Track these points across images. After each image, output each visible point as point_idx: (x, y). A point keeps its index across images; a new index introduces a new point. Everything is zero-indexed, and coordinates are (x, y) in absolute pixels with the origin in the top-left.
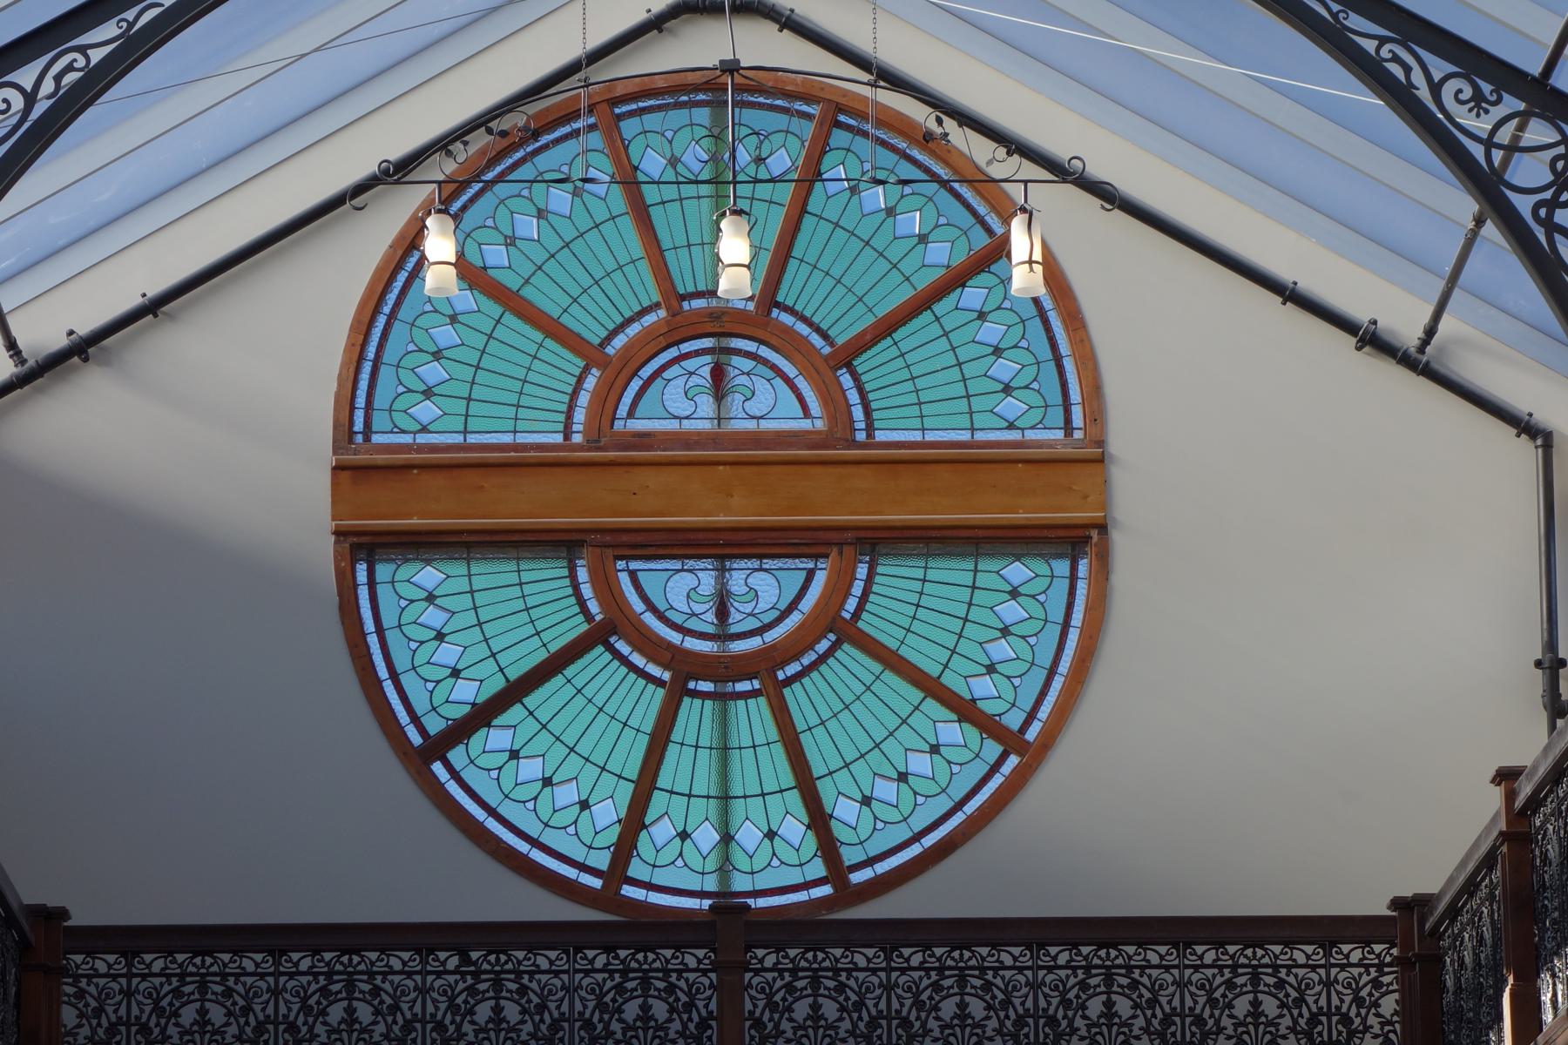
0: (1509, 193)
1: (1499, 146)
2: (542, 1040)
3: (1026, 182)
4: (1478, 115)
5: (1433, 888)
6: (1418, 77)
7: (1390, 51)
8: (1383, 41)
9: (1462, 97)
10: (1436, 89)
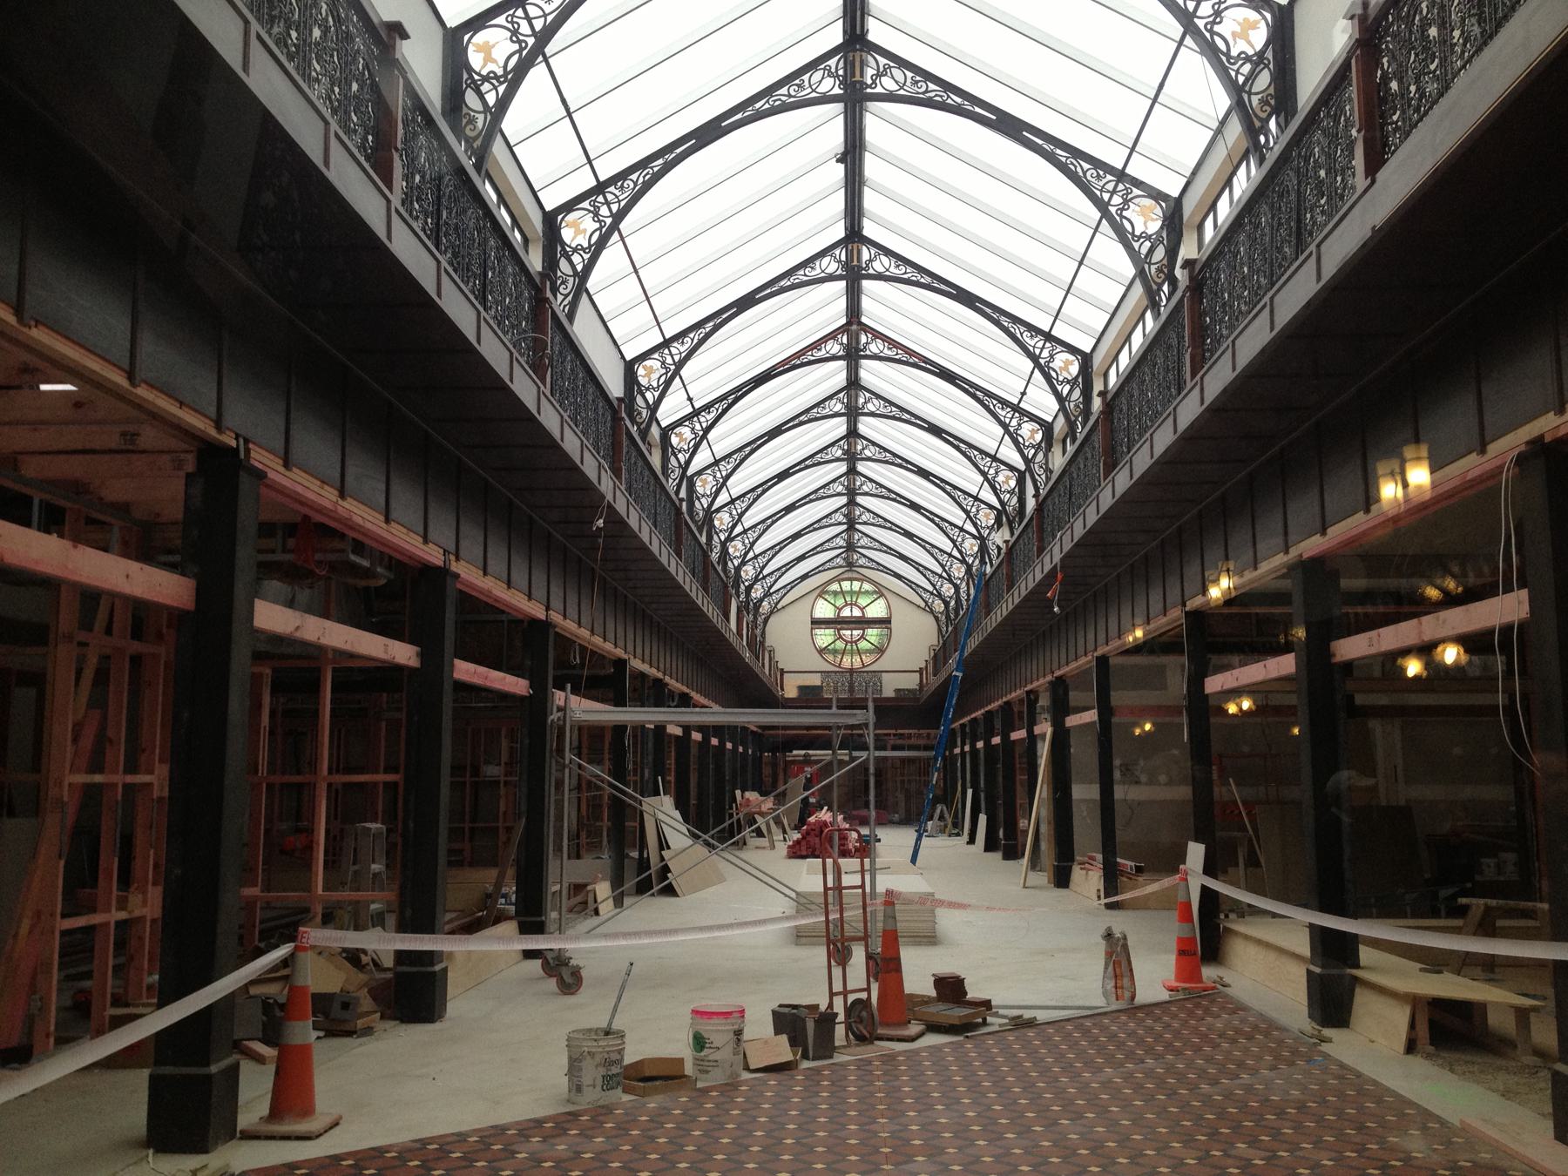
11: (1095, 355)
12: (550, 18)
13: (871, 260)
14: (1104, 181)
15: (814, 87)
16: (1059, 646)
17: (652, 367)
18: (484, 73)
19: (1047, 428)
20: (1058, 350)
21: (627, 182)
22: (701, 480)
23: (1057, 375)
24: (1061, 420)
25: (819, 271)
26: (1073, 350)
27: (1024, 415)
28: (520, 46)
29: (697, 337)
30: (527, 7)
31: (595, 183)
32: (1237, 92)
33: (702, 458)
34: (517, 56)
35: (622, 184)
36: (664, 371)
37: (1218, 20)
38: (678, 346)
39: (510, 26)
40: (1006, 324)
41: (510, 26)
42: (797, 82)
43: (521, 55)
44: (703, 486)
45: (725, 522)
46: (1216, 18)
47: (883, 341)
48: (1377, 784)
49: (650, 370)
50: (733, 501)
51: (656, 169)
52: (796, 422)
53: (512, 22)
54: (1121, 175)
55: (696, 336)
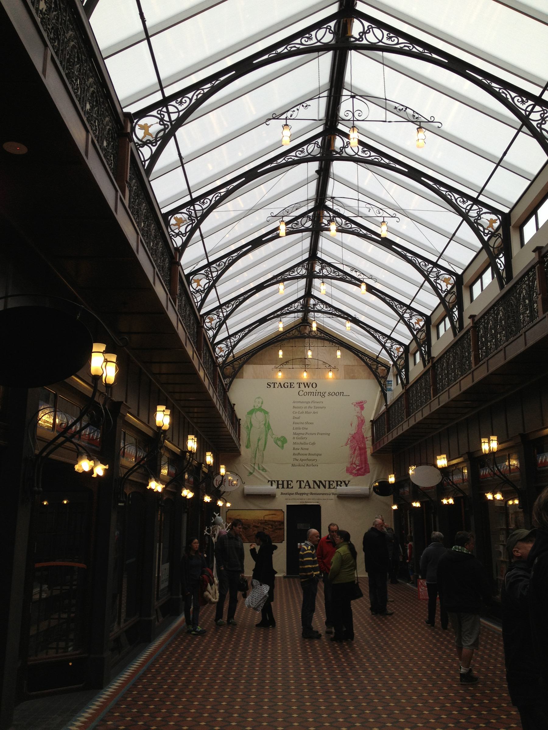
0: (430, 278)
1: (467, 210)
2: (313, 268)
3: (384, 217)
4: (523, 105)
5: (477, 314)
6: (453, 198)
7: (502, 91)
8: (447, 192)
9: (519, 101)
10: (456, 200)
11: (410, 346)
12: (181, 113)
13: (364, 33)
15: (296, 307)
18: (197, 289)
19: (407, 348)
20: (394, 344)
21: (230, 305)
22: (209, 318)
23: (394, 354)
24: (414, 344)
25: (314, 40)
26: (401, 344)
27: (379, 364)
29: (241, 335)
30: (169, 107)
31: (162, 98)
32: (443, 300)
33: (211, 304)
34: (219, 323)
35: (182, 99)
36: (219, 320)
37: (544, 122)
38: (233, 339)
39: (159, 116)
40: (372, 332)
41: (159, 116)
42: (300, 149)
43: (165, 132)
46: (478, 218)
49: (221, 350)
50: (229, 337)
51: (206, 91)
53: (160, 114)
54: (409, 307)
55: (241, 334)
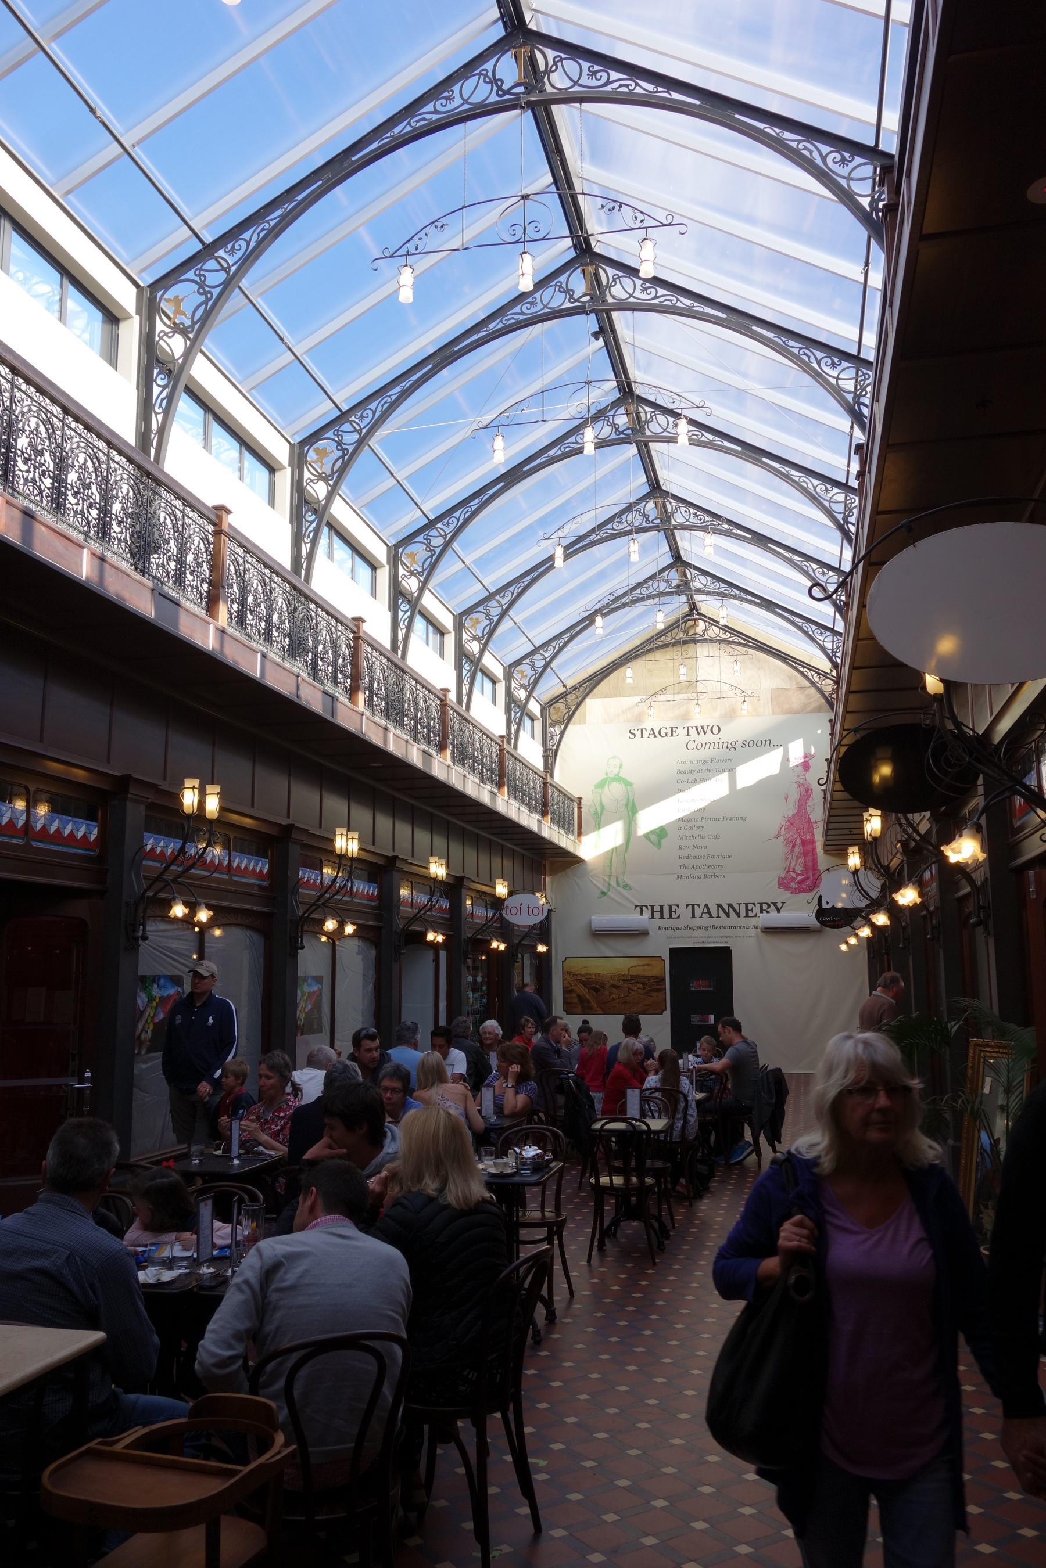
14: (827, 576)
16: (454, 1181)
17: (324, 450)
25: (458, 101)
28: (206, 297)
35: (362, 414)
44: (320, 460)
45: (188, 307)
47: (705, 621)
48: (320, 990)
52: (386, 139)
